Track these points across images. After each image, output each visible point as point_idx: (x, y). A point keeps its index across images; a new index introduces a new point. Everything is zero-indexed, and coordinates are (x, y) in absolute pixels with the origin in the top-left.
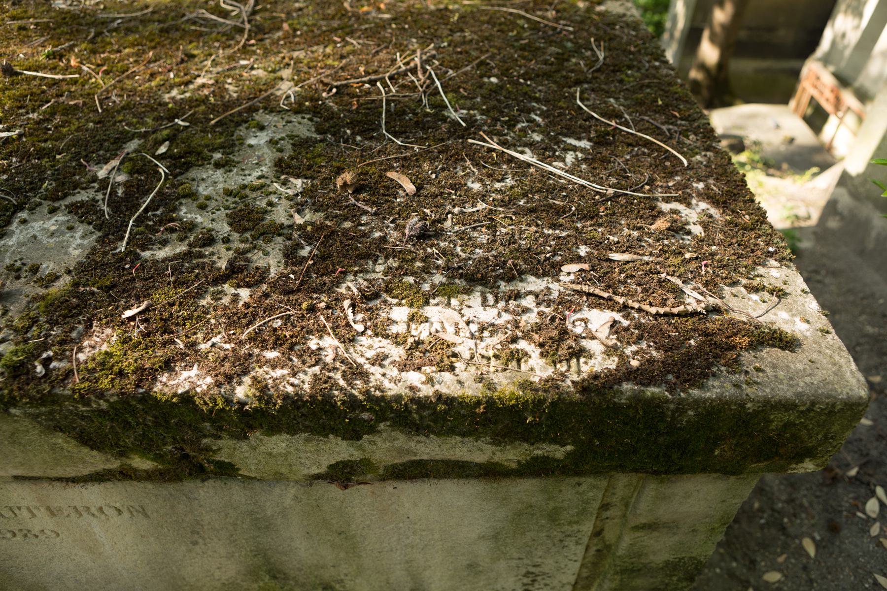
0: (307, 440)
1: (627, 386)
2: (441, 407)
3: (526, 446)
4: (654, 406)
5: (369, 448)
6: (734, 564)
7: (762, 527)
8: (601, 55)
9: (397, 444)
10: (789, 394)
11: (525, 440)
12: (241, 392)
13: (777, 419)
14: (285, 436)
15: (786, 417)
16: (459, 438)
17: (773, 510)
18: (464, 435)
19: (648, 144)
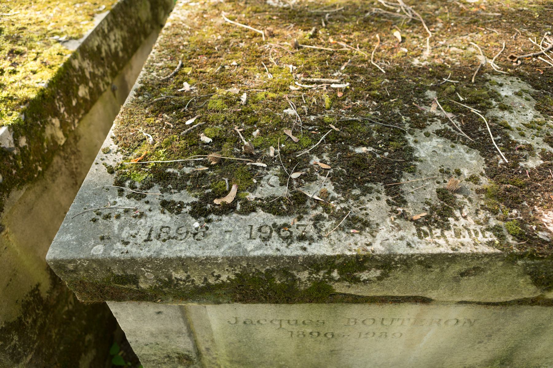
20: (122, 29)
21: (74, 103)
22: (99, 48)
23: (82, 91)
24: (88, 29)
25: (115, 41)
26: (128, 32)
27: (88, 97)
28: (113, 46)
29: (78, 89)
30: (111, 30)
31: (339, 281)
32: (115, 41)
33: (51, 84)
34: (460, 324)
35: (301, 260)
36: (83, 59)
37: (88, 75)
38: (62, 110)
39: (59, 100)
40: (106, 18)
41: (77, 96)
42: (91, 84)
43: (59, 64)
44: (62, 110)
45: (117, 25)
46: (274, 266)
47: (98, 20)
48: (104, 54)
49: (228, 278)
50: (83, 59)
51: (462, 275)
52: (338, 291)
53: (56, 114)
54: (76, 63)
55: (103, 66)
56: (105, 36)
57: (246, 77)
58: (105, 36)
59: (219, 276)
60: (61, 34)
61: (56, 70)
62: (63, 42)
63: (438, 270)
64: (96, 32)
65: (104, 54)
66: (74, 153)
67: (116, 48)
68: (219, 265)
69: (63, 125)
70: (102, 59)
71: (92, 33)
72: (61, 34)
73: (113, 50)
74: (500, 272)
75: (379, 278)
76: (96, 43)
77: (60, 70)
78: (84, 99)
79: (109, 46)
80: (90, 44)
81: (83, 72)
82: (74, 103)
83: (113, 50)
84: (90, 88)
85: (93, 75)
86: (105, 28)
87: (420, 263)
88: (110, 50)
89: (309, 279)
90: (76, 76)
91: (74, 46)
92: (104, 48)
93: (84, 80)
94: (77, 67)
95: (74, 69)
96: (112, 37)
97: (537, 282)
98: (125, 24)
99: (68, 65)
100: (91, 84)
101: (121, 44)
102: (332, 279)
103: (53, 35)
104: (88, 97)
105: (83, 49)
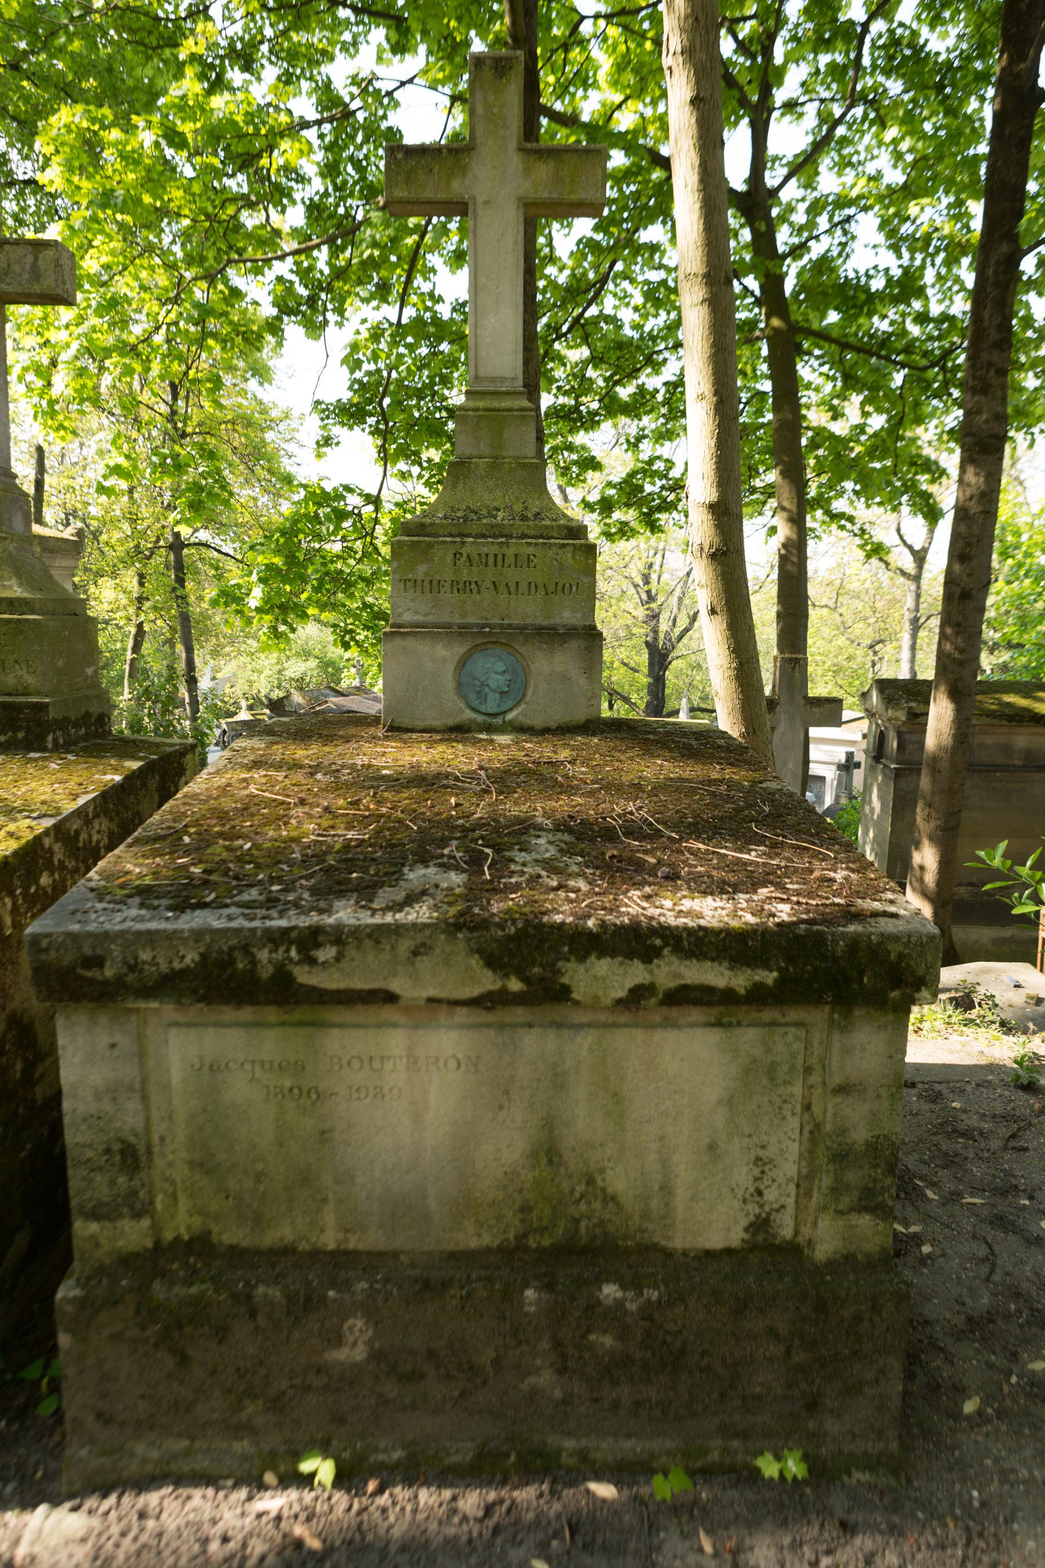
0: (621, 964)
1: (803, 926)
2: (701, 934)
3: (749, 971)
4: (821, 934)
5: (656, 971)
6: (993, 1358)
7: (1021, 1326)
8: (767, 809)
9: (673, 968)
10: (894, 931)
11: (748, 965)
12: (590, 923)
13: (895, 949)
14: (608, 960)
15: (900, 948)
16: (709, 963)
17: (1032, 1310)
18: (713, 960)
19: (805, 848)
20: (111, 820)
21: (33, 890)
22: (77, 833)
23: (45, 880)
24: (69, 807)
25: (99, 832)
26: (118, 825)
27: (49, 890)
28: (95, 838)
29: (40, 875)
30: (96, 816)
31: (298, 963)
32: (99, 832)
33: (15, 853)
34: (463, 1068)
35: (259, 933)
36: (56, 841)
37: (56, 863)
38: (18, 891)
39: (19, 877)
40: (94, 799)
41: (37, 883)
42: (57, 876)
43: (28, 836)
44: (18, 891)
45: (106, 812)
46: (233, 942)
47: (82, 801)
48: (81, 844)
49: (193, 961)
50: (56, 841)
51: (415, 953)
52: (300, 980)
53: (11, 894)
54: (47, 842)
55: (77, 859)
56: (88, 822)
57: (257, 833)
58: (88, 822)
59: (183, 957)
60: (33, 811)
61: (23, 841)
62: (35, 818)
63: (388, 947)
64: (78, 812)
65: (81, 844)
66: (13, 963)
67: (98, 842)
68: (185, 940)
69: (15, 911)
70: (78, 849)
71: (73, 813)
72: (33, 811)
73: (94, 844)
74: (448, 949)
75: (337, 959)
76: (75, 827)
77: (28, 842)
78: (43, 888)
79: (90, 836)
80: (68, 824)
81: (52, 857)
82: (33, 890)
83: (94, 844)
84: (54, 880)
85: (62, 866)
86: (91, 810)
87: (369, 936)
88: (90, 841)
89: (270, 961)
90: (42, 857)
91: (48, 823)
92: (83, 836)
93: (49, 867)
94: (47, 846)
95: (43, 848)
96: (97, 827)
97: (491, 962)
98: (118, 814)
99: (38, 839)
100: (57, 876)
101: (106, 840)
102: (291, 960)
103: (21, 811)
104: (49, 890)
105: (57, 827)
